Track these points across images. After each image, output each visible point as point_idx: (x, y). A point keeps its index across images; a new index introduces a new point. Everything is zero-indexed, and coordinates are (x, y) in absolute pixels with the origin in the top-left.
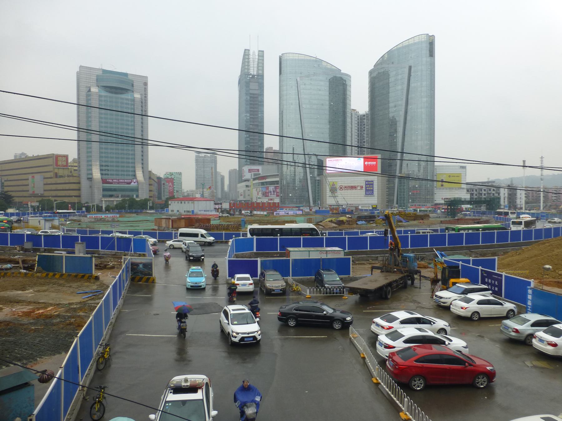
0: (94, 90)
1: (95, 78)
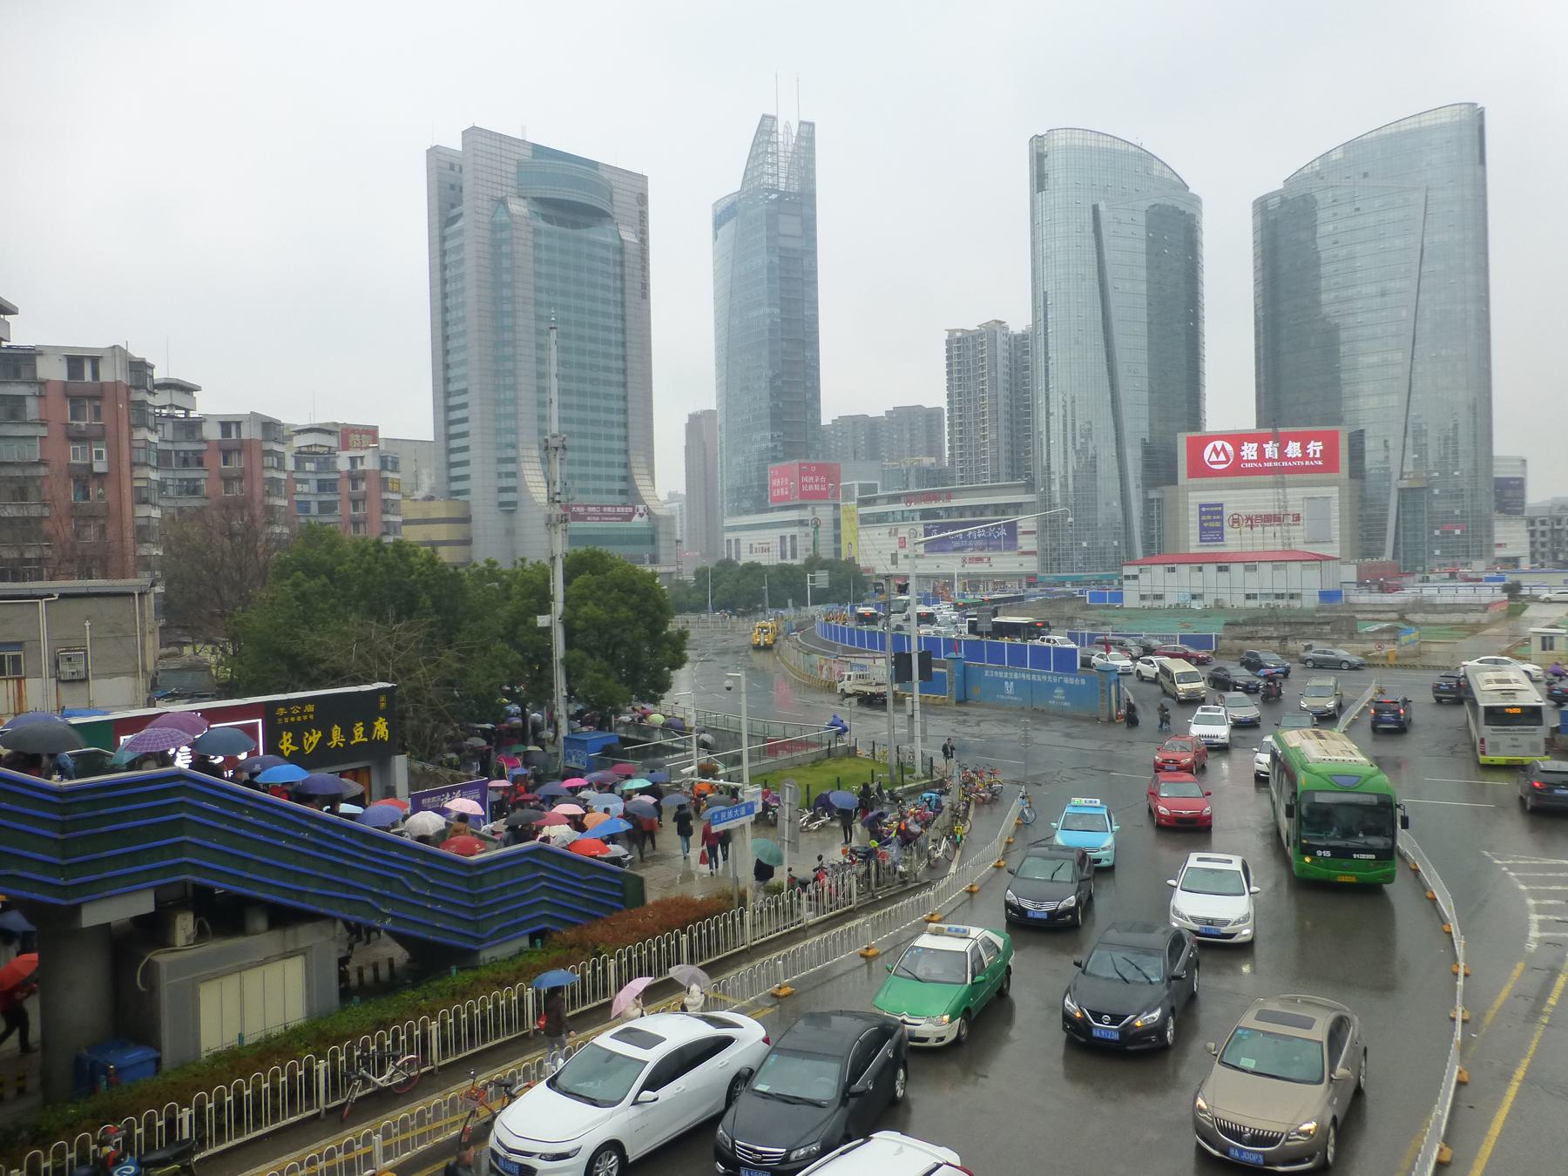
0: (518, 207)
1: (513, 169)
